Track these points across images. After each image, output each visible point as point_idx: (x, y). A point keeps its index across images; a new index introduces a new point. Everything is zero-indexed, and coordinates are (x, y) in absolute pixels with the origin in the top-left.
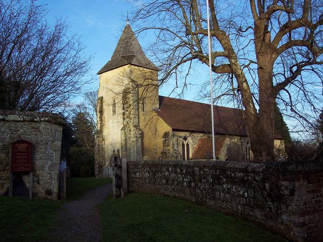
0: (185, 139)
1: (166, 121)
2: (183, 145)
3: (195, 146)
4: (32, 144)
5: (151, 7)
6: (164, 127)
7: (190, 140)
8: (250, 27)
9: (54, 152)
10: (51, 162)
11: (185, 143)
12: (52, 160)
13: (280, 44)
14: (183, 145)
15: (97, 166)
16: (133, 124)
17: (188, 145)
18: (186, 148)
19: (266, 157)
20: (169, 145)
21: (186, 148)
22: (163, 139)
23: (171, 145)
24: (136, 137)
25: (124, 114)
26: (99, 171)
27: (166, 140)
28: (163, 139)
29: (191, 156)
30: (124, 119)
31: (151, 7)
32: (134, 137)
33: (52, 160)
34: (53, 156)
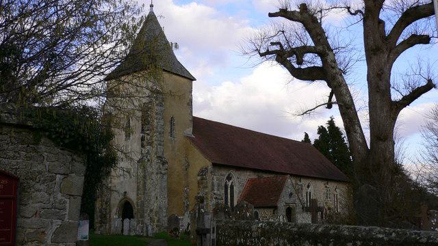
0: (229, 178)
1: (203, 152)
2: (226, 186)
3: (242, 189)
4: (17, 179)
5: (77, 82)
6: (200, 161)
7: (234, 179)
8: (360, 11)
9: (68, 201)
10: (60, 222)
11: (230, 184)
12: (61, 218)
13: (400, 40)
14: (226, 186)
15: (99, 214)
16: (156, 154)
17: (232, 187)
18: (229, 191)
19: (122, 191)
20: (206, 187)
21: (229, 191)
22: (199, 178)
23: (210, 188)
24: (161, 173)
25: (143, 139)
26: (101, 222)
27: (202, 179)
28: (199, 178)
29: (235, 203)
30: (143, 146)
31: (77, 82)
32: (157, 174)
33: (61, 218)
34: (64, 209)
